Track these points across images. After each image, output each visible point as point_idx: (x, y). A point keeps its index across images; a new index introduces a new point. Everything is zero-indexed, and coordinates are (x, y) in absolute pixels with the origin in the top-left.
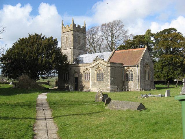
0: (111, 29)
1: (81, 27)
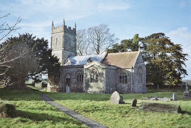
0: (97, 32)
1: (72, 29)
